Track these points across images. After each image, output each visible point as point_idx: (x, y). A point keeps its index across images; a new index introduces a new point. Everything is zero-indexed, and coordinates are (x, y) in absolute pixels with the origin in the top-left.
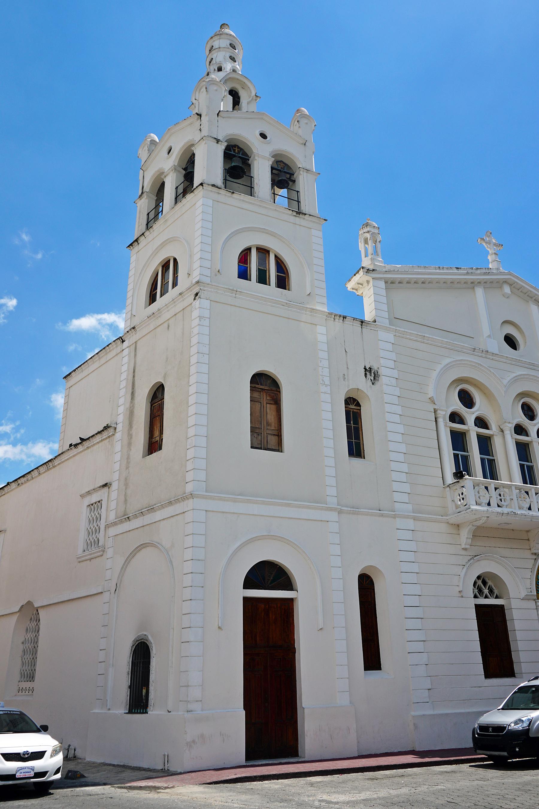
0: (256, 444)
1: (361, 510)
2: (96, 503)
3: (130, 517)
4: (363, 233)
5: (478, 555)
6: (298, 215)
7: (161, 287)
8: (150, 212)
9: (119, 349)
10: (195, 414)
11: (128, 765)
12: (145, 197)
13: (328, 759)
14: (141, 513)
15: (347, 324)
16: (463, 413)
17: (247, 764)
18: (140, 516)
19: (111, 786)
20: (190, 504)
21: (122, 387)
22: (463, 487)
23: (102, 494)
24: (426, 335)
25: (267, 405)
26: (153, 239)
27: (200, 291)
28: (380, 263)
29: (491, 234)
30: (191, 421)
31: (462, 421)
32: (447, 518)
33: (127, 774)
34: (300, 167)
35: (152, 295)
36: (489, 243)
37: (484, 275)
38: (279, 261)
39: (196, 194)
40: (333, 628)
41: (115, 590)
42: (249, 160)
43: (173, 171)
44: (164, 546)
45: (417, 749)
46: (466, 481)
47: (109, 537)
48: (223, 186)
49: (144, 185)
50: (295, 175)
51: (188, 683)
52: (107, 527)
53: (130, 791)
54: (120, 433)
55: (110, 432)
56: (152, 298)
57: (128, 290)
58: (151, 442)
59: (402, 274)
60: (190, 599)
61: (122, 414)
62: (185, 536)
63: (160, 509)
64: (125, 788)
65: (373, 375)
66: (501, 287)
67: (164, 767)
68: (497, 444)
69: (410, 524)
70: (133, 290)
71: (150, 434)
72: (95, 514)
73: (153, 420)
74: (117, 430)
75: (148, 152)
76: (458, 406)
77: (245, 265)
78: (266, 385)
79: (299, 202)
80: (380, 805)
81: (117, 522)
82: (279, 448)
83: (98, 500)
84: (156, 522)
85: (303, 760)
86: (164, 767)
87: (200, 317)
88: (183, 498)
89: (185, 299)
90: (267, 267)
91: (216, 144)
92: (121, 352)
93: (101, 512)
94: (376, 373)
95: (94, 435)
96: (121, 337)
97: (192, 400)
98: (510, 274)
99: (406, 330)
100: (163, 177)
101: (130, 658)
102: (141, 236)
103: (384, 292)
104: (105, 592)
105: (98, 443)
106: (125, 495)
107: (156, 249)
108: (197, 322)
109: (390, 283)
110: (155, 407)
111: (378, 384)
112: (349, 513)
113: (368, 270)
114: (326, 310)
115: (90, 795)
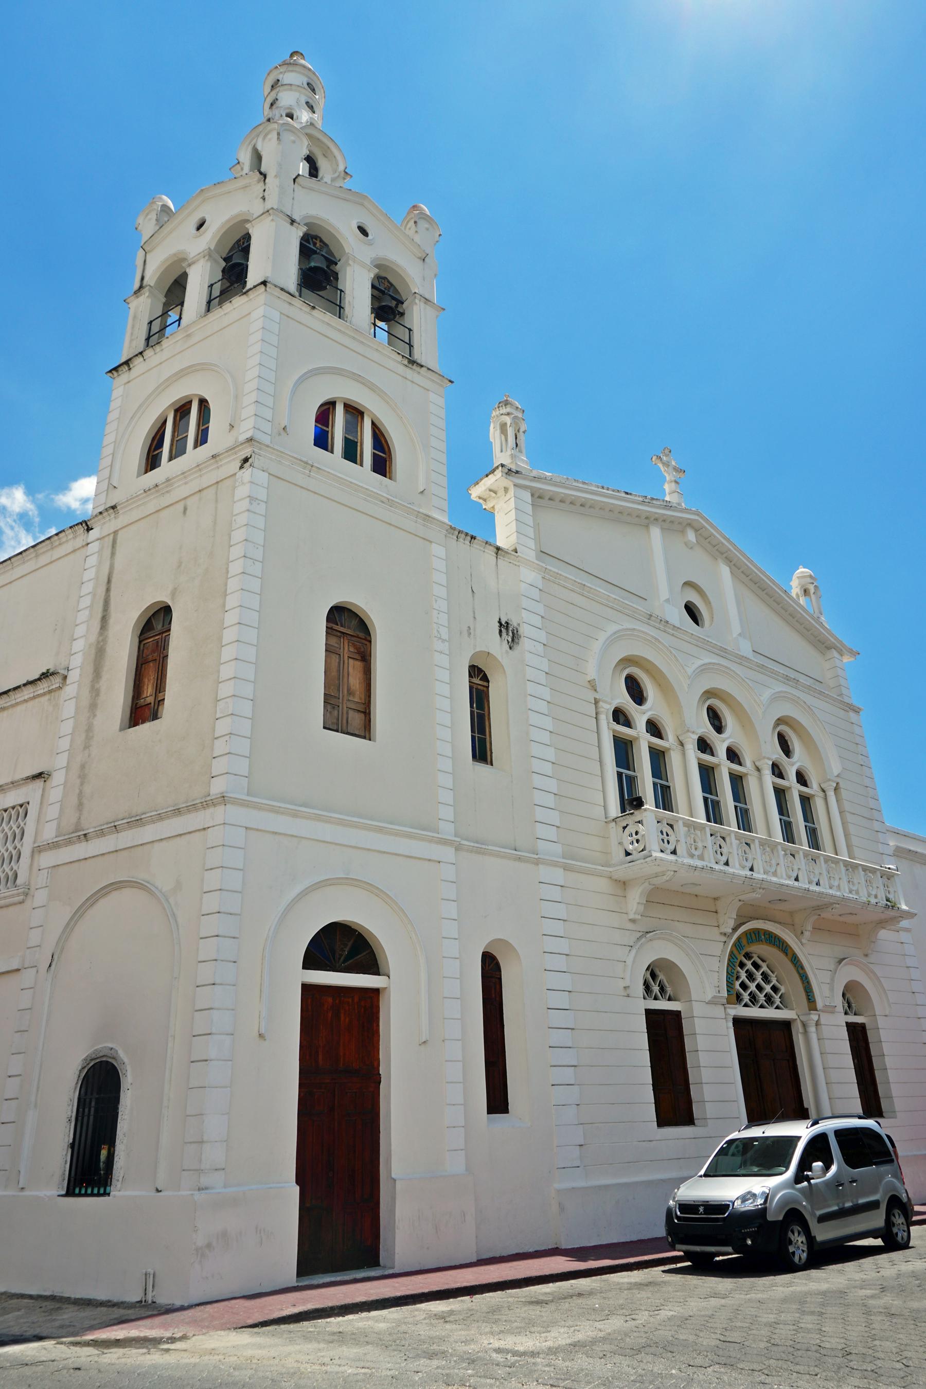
0: (330, 723)
1: (490, 847)
2: (13, 808)
3: (89, 833)
4: (498, 416)
5: (650, 932)
6: (410, 366)
7: (172, 445)
8: (154, 320)
9: (79, 542)
10: (236, 659)
11: (61, 1295)
12: (147, 294)
13: (430, 1268)
14: (114, 828)
15: (477, 548)
16: (631, 711)
17: (300, 1284)
18: (111, 833)
19: (55, 1342)
20: (218, 814)
21: (82, 606)
22: (639, 822)
23: (32, 791)
24: (586, 584)
25: (350, 660)
26: (161, 363)
27: (253, 454)
28: (523, 463)
29: (670, 452)
30: (227, 671)
31: (628, 723)
32: (611, 869)
33: (68, 1315)
34: (415, 293)
35: (150, 457)
36: (667, 465)
37: (664, 509)
38: (377, 432)
39: (251, 297)
40: (443, 1041)
41: (50, 966)
42: (336, 264)
43: (207, 258)
44: (160, 888)
45: (564, 1246)
46: (645, 814)
47: (39, 870)
48: (297, 294)
49: (144, 275)
50: (405, 306)
51: (202, 1136)
52: (38, 850)
53: (105, 1351)
54: (76, 685)
55: (53, 682)
56: (152, 461)
57: (105, 443)
58: (136, 705)
59: (555, 485)
60: (213, 983)
61: (81, 653)
62: (206, 870)
63: (153, 822)
64: (87, 1344)
65: (511, 634)
66: (683, 532)
67: (145, 1297)
68: (674, 761)
69: (558, 876)
70: (115, 445)
71: (134, 691)
72: (11, 828)
73: (141, 667)
74: (68, 681)
75: (156, 224)
76: (624, 699)
77: (325, 428)
78: (349, 628)
79: (411, 346)
80: (615, 1354)
81: (163, 815)
82: (366, 732)
83: (21, 802)
84: (144, 844)
85: (391, 1272)
86: (145, 1297)
87: (252, 499)
88: (205, 803)
89: (221, 466)
90: (359, 438)
91: (288, 225)
92: (83, 547)
93: (25, 824)
94: (515, 632)
95: (19, 687)
96: (85, 522)
97: (229, 635)
98: (698, 514)
99: (560, 572)
100: (184, 265)
101: (74, 1092)
102: (137, 355)
103: (529, 509)
104: (25, 968)
105: (25, 701)
106: (80, 795)
107: (167, 380)
108: (245, 504)
109: (538, 497)
110: (148, 644)
111: (518, 649)
112: (471, 850)
113: (510, 470)
114: (446, 521)
115: (27, 1365)
